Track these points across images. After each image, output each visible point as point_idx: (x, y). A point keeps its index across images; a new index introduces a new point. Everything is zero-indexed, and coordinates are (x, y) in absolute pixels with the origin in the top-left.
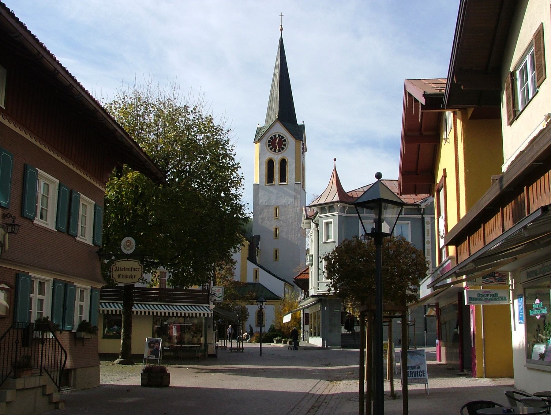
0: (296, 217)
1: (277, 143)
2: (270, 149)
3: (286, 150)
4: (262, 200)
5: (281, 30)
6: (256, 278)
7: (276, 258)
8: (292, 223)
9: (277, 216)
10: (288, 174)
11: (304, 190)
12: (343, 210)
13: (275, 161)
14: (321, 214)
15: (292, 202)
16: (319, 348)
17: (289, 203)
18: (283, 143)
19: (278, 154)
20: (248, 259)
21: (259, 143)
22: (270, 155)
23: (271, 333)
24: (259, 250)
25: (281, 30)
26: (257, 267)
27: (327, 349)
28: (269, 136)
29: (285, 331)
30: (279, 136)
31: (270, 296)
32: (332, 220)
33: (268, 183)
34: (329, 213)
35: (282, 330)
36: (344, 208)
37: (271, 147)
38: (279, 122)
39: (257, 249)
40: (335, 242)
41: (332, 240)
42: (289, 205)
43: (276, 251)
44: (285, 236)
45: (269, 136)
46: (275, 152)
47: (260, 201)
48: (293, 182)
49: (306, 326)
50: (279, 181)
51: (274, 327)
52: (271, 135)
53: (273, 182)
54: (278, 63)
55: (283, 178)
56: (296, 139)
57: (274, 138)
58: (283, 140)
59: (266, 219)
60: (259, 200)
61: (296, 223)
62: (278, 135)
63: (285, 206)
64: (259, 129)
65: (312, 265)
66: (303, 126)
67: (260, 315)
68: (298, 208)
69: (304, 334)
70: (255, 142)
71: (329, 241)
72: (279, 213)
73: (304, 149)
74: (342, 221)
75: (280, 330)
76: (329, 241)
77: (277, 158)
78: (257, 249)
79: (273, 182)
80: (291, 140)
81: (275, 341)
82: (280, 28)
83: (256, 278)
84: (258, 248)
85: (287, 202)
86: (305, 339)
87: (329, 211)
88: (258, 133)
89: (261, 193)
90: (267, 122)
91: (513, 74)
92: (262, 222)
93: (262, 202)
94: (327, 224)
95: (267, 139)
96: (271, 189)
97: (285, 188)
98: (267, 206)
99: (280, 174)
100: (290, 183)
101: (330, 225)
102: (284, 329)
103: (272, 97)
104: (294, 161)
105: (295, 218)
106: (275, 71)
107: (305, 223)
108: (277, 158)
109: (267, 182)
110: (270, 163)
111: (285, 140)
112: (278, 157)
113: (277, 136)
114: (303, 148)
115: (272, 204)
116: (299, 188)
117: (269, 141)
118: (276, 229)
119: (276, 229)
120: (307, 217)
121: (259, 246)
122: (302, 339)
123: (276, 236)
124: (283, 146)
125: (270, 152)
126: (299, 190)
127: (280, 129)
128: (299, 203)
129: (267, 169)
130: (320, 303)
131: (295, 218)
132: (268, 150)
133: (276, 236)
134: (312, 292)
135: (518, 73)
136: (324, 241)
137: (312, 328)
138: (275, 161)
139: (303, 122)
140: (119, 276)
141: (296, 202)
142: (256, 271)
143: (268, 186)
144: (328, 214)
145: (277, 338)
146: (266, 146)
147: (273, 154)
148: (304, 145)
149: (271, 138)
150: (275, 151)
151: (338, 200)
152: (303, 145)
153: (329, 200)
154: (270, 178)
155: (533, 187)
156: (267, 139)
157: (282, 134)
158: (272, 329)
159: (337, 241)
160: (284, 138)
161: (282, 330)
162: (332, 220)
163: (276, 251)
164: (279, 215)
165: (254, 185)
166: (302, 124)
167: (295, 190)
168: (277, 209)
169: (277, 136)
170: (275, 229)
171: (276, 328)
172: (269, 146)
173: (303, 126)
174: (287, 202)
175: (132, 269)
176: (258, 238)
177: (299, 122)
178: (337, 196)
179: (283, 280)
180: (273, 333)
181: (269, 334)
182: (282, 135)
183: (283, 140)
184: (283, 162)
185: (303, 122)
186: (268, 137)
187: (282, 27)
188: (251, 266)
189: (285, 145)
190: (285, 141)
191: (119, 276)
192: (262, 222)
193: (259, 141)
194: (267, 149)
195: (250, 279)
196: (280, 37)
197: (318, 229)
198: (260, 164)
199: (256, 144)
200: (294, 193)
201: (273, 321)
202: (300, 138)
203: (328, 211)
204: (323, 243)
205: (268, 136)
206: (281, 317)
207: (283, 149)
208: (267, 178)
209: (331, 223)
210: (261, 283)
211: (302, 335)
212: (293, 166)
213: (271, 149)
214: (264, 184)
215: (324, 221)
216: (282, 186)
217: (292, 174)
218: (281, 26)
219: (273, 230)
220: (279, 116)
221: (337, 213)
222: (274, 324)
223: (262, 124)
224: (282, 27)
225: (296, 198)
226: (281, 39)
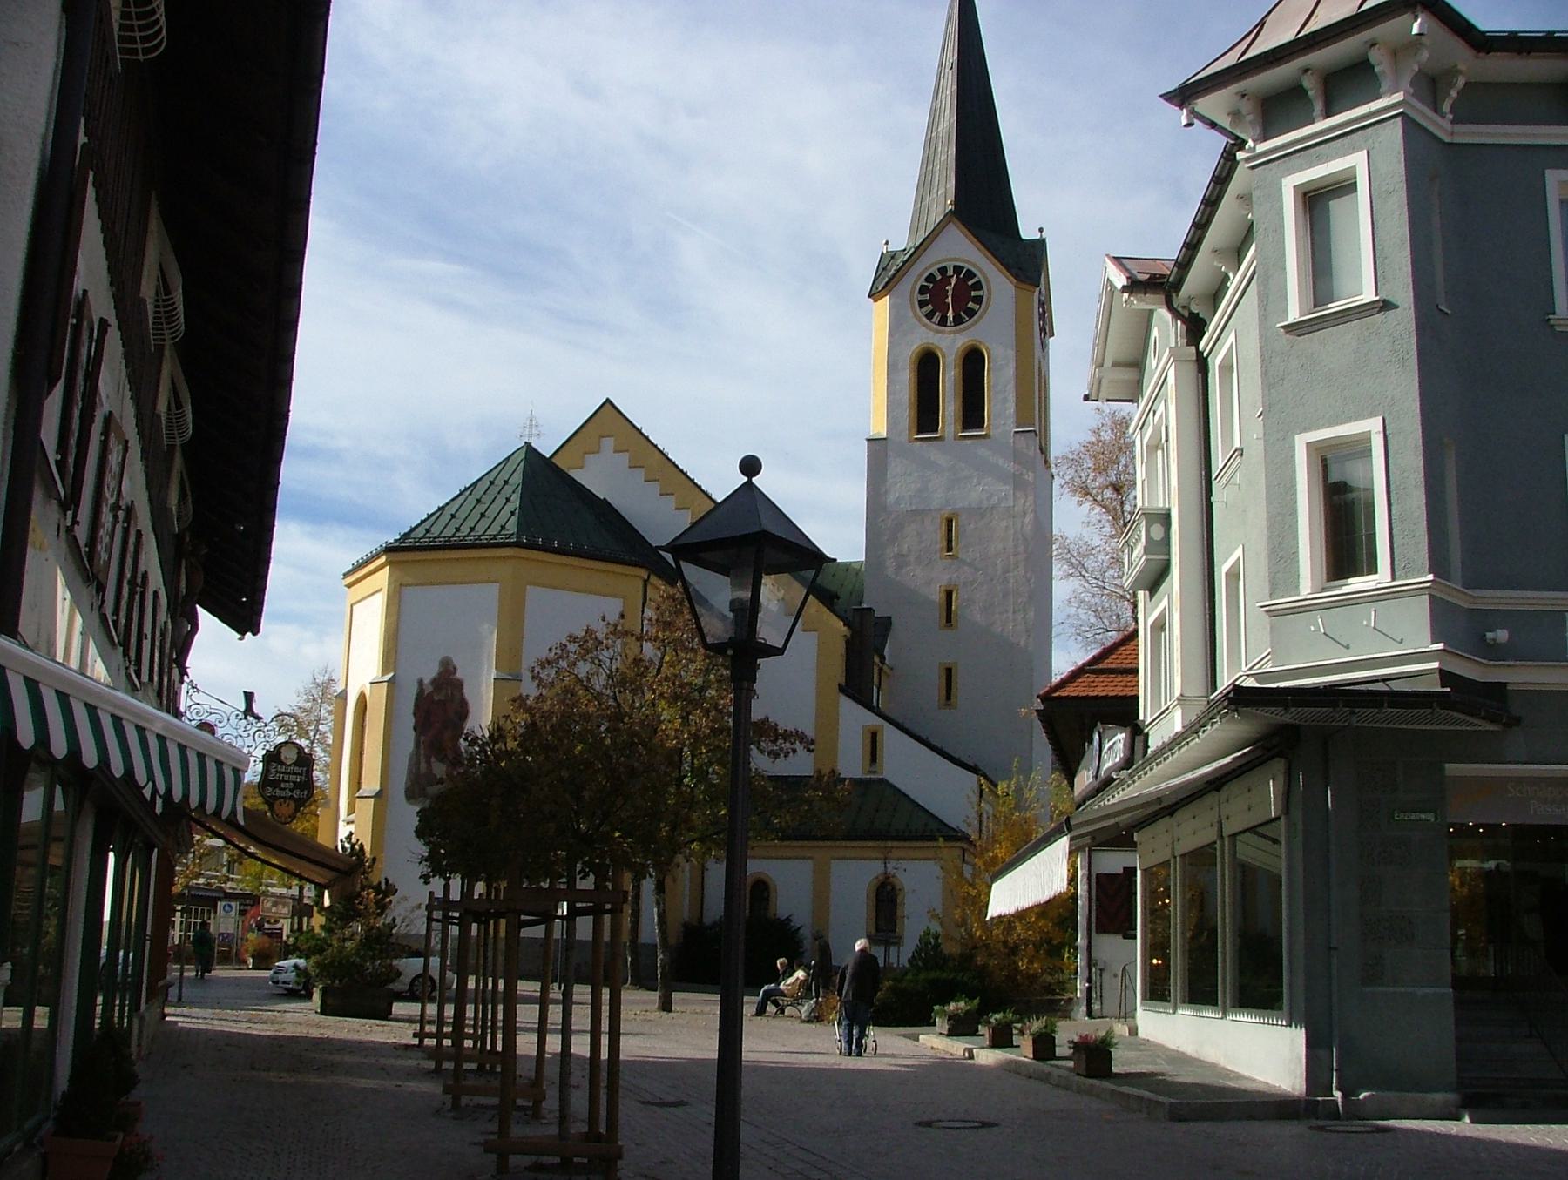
0: (1021, 549)
1: (950, 293)
2: (926, 316)
3: (981, 317)
4: (900, 490)
6: (874, 757)
7: (948, 697)
8: (1006, 571)
9: (949, 549)
10: (989, 401)
13: (944, 357)
14: (1265, 139)
16: (1275, 1108)
17: (995, 500)
18: (973, 293)
19: (954, 332)
20: (842, 690)
22: (925, 335)
23: (922, 976)
24: (885, 668)
26: (875, 720)
27: (1354, 1111)
28: (923, 272)
29: (993, 962)
30: (958, 269)
31: (926, 825)
33: (919, 432)
34: (1328, 115)
35: (979, 960)
37: (930, 307)
38: (959, 224)
39: (876, 659)
40: (1385, 306)
42: (993, 507)
43: (949, 671)
44: (979, 618)
46: (946, 326)
47: (891, 498)
48: (1007, 428)
49: (1109, 945)
50: (959, 427)
51: (937, 945)
52: (930, 267)
53: (936, 431)
55: (972, 414)
57: (939, 277)
58: (970, 283)
59: (912, 559)
60: (886, 492)
61: (1021, 570)
62: (955, 267)
63: (980, 512)
64: (887, 259)
67: (886, 899)
68: (1027, 520)
69: (1089, 980)
70: (874, 295)
72: (957, 537)
75: (966, 960)
77: (950, 345)
78: (876, 659)
79: (936, 431)
80: (999, 286)
81: (942, 1024)
83: (874, 757)
84: (883, 658)
85: (989, 498)
86: (1096, 1007)
88: (884, 269)
89: (896, 467)
90: (913, 232)
92: (899, 567)
93: (897, 502)
94: (1315, 200)
95: (916, 283)
96: (932, 452)
97: (982, 450)
98: (915, 513)
100: (1000, 430)
101: (1336, 206)
102: (991, 955)
103: (932, 149)
104: (1011, 353)
105: (1015, 554)
107: (1108, 363)
108: (950, 345)
109: (914, 430)
110: (927, 364)
113: (950, 273)
114: (1043, 330)
115: (935, 505)
117: (923, 290)
118: (949, 594)
119: (949, 594)
121: (886, 652)
122: (1084, 1009)
123: (949, 619)
124: (970, 304)
125: (925, 325)
126: (1031, 453)
127: (962, 249)
128: (1031, 499)
129: (914, 385)
130: (1279, 766)
131: (1015, 554)
132: (920, 320)
133: (949, 619)
136: (1294, 315)
138: (944, 357)
139: (1041, 230)
141: (1018, 495)
142: (874, 736)
143: (919, 443)
145: (952, 1006)
146: (913, 307)
147: (938, 332)
148: (1045, 306)
149: (930, 278)
152: (1042, 304)
154: (926, 417)
158: (929, 953)
159: (1404, 296)
161: (979, 960)
162: (1356, 161)
163: (949, 671)
164: (957, 544)
165: (868, 440)
166: (1038, 237)
167: (1017, 457)
168: (950, 521)
169: (950, 273)
170: (943, 595)
171: (950, 948)
172: (922, 304)
173: (1040, 245)
174: (989, 498)
176: (885, 624)
177: (1027, 232)
179: (974, 769)
180: (933, 975)
181: (909, 977)
182: (967, 266)
183: (970, 283)
184: (973, 362)
185: (1041, 230)
186: (921, 275)
188: (853, 718)
190: (978, 286)
192: (899, 567)
195: (851, 765)
197: (1199, 354)
198: (892, 368)
199: (876, 301)
200: (1010, 467)
201: (935, 916)
203: (1318, 107)
204: (1290, 328)
205: (918, 273)
206: (973, 892)
208: (914, 414)
209: (1343, 186)
210: (891, 780)
211: (1081, 985)
212: (1010, 371)
213: (929, 316)
214: (904, 437)
216: (969, 442)
217: (1005, 400)
219: (937, 596)
220: (956, 202)
221: (1399, 97)
222: (935, 927)
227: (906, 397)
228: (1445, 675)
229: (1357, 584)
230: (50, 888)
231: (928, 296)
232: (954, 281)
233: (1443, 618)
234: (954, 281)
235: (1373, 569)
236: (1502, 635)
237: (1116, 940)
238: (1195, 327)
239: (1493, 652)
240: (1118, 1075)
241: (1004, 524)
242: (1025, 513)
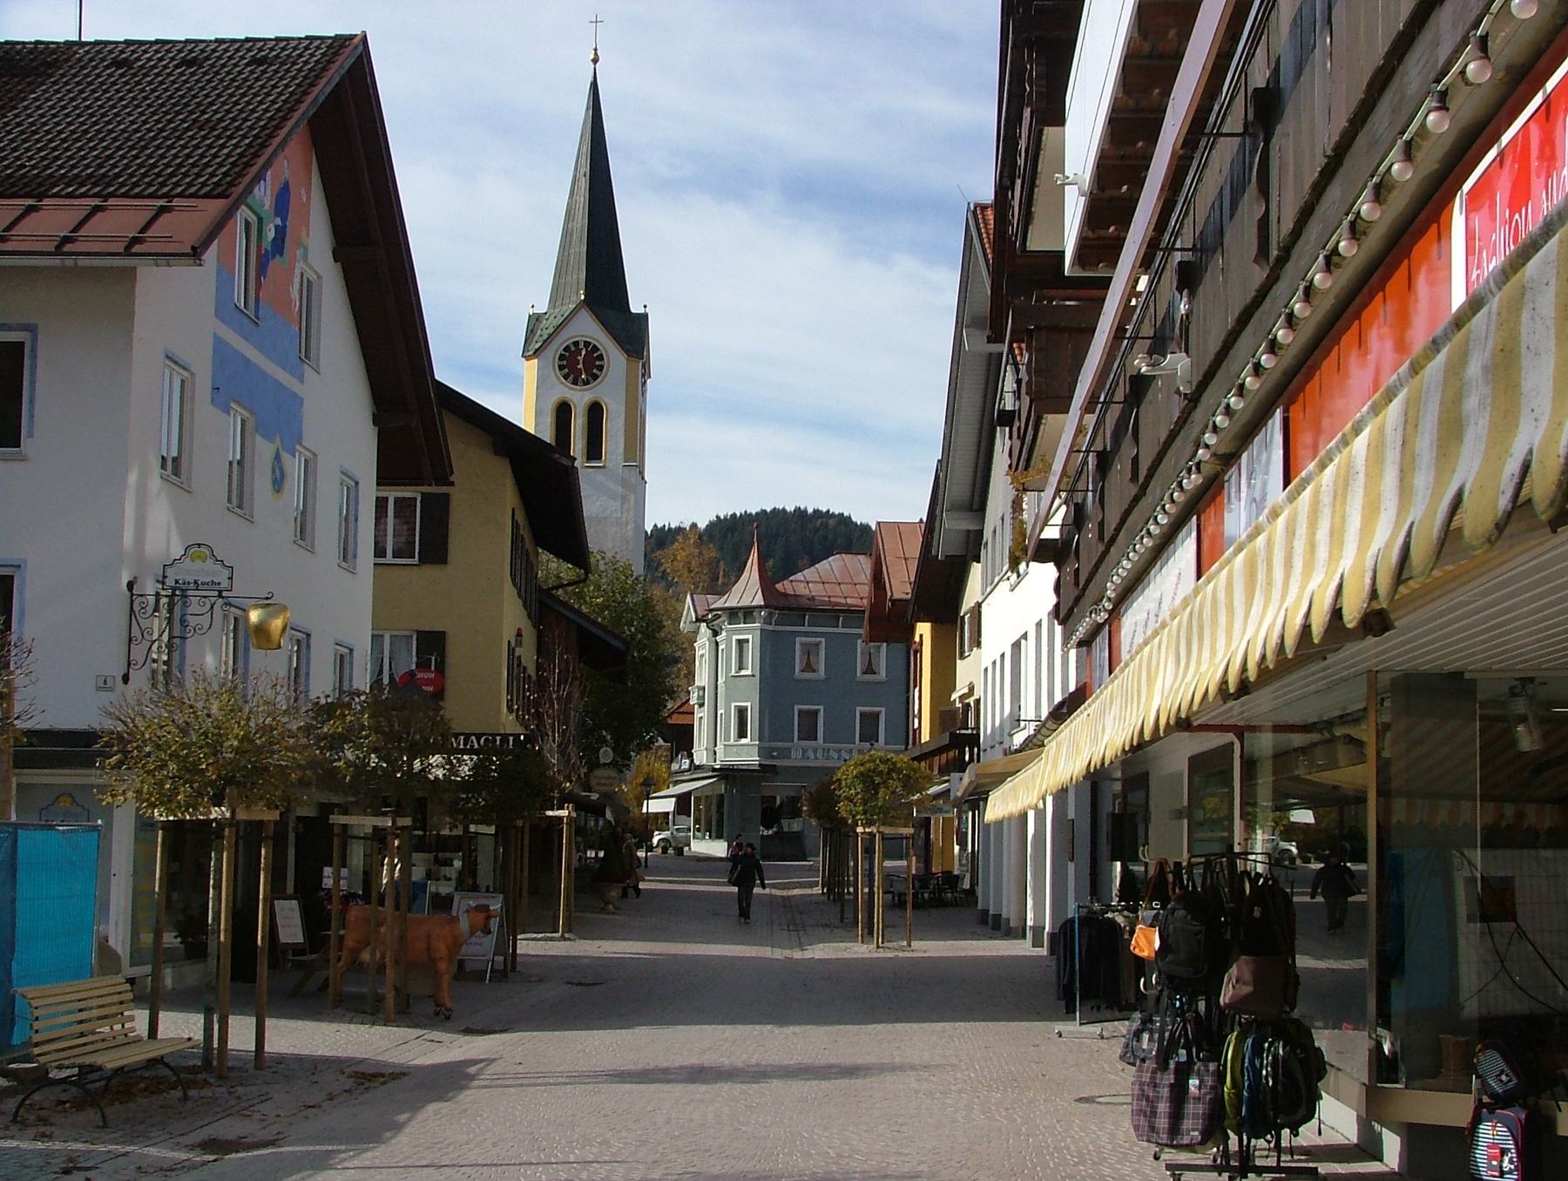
5: (595, 61)
11: (643, 478)
12: (767, 620)
13: (575, 407)
15: (616, 511)
16: (721, 859)
17: (608, 512)
19: (584, 390)
21: (536, 360)
25: (595, 61)
30: (587, 344)
32: (750, 637)
36: (770, 614)
37: (566, 370)
40: (753, 676)
41: (749, 672)
45: (563, 343)
52: (566, 341)
54: (585, 149)
56: (627, 352)
57: (573, 349)
65: (701, 705)
66: (645, 316)
68: (629, 527)
71: (743, 673)
73: (646, 373)
74: (767, 639)
76: (743, 673)
77: (580, 399)
82: (592, 57)
85: (603, 511)
87: (745, 618)
91: (963, 618)
94: (741, 643)
95: (557, 351)
99: (585, 441)
104: (623, 408)
106: (576, 169)
108: (580, 399)
111: (601, 355)
112: (582, 397)
113: (581, 346)
114: (643, 375)
116: (634, 479)
117: (562, 357)
120: (697, 618)
124: (595, 371)
125: (562, 383)
127: (589, 329)
134: (701, 756)
135: (966, 617)
136: (733, 673)
137: (703, 822)
139: (645, 307)
140: (598, 784)
144: (742, 625)
146: (554, 370)
149: (567, 349)
150: (575, 382)
151: (762, 603)
152: (644, 366)
153: (745, 602)
155: (1439, 228)
156: (557, 351)
157: (594, 339)
160: (598, 349)
166: (642, 311)
167: (624, 483)
169: (581, 346)
175: (610, 778)
177: (635, 308)
178: (759, 596)
184: (595, 411)
185: (645, 307)
187: (596, 54)
189: (601, 368)
190: (601, 357)
191: (598, 784)
193: (536, 353)
194: (555, 376)
196: (590, 79)
200: (620, 490)
202: (637, 353)
207: (595, 377)
209: (747, 641)
212: (621, 422)
213: (566, 377)
215: (735, 637)
216: (591, 470)
218: (596, 50)
223: (542, 307)
224: (596, 54)
225: (624, 498)
226: (594, 85)
227: (549, 420)
228: (760, 765)
229: (744, 741)
230: (1227, 903)
231: (565, 363)
232: (583, 353)
233: (762, 751)
234: (583, 353)
235: (746, 737)
236: (775, 754)
237: (684, 817)
238: (715, 633)
239: (773, 757)
240: (1041, 132)
241: (614, 529)
242: (627, 524)
